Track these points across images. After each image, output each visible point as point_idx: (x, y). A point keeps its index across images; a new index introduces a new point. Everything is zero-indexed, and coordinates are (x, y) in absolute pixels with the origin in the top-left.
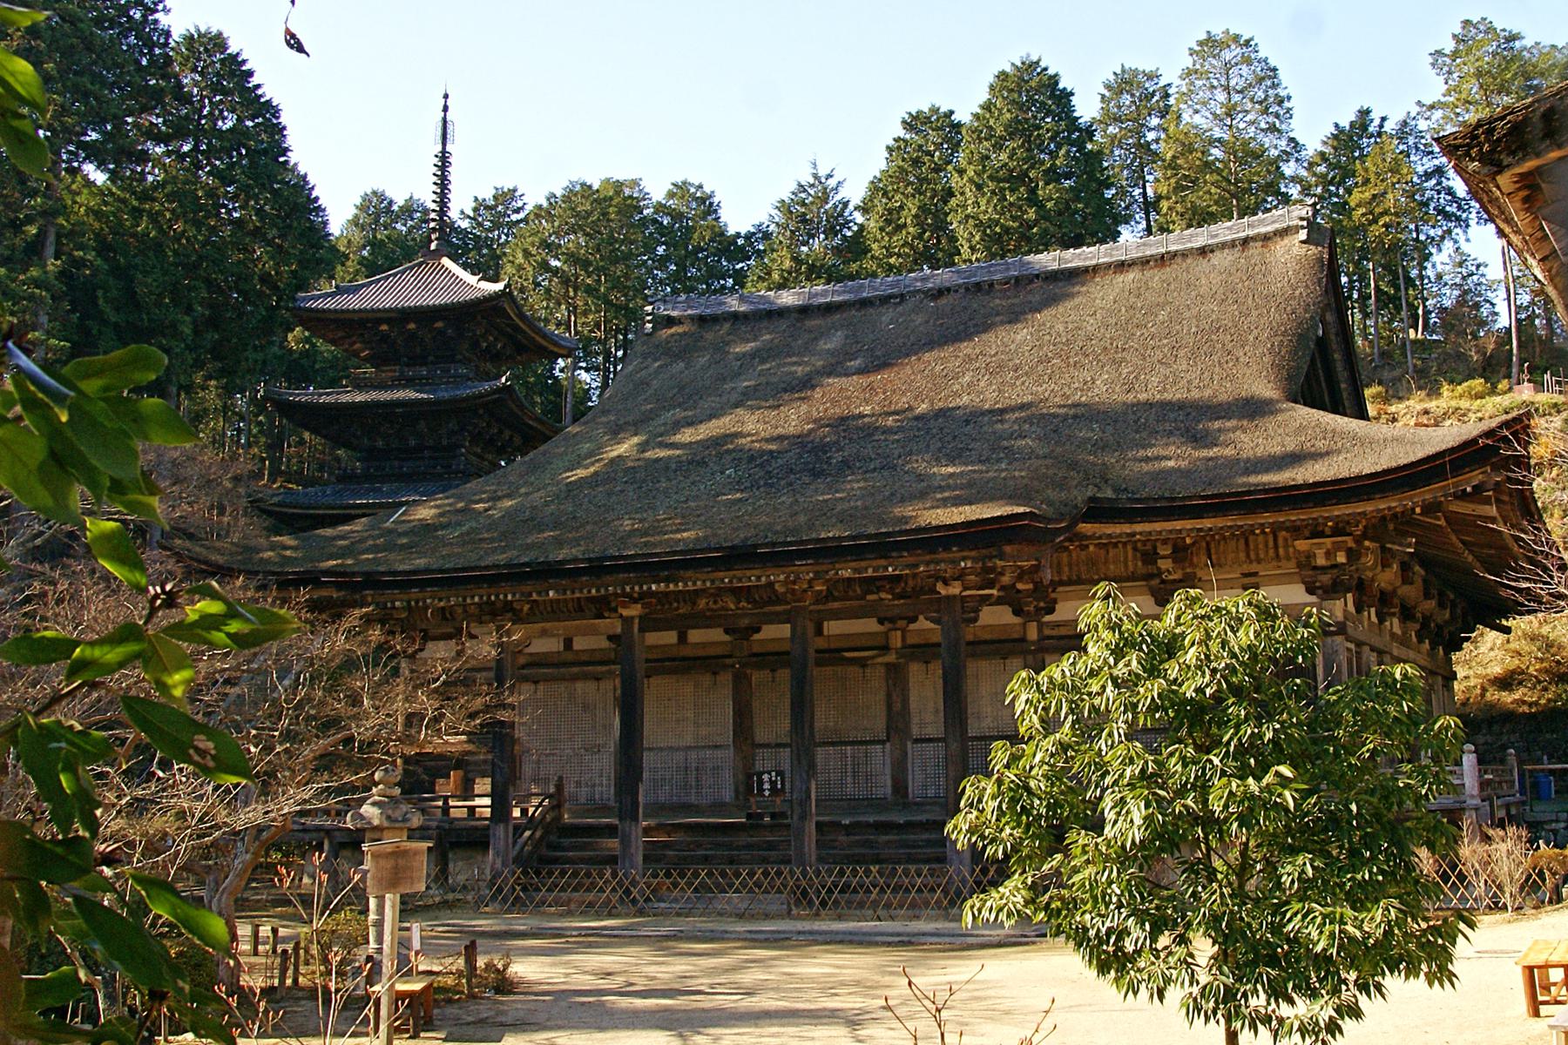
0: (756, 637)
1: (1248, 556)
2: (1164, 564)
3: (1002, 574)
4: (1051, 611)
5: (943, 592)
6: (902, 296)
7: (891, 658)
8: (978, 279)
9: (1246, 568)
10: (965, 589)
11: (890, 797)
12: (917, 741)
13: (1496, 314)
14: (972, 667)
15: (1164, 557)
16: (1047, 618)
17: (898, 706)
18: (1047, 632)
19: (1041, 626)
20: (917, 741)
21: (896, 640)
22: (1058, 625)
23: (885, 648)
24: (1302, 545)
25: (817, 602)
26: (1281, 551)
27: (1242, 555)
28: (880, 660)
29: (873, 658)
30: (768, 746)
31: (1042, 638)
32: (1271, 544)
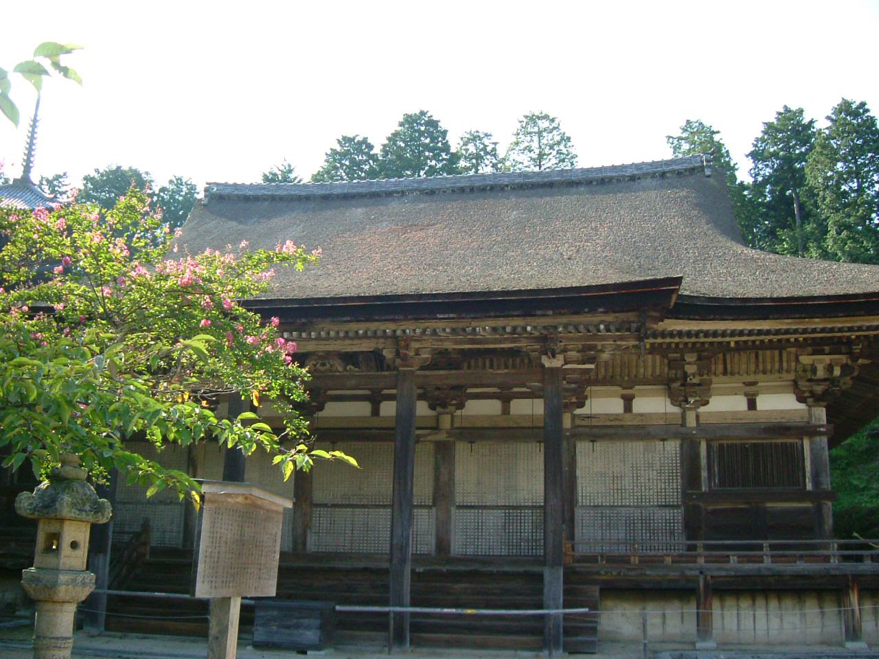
0: (321, 414)
1: (757, 366)
2: (691, 369)
3: (602, 351)
4: (581, 405)
5: (547, 365)
6: (403, 192)
7: (442, 437)
8: (462, 185)
9: (751, 378)
10: (566, 363)
11: (433, 553)
12: (459, 507)
13: (554, 356)
14: (314, 502)
15: (689, 363)
16: (578, 411)
17: (444, 478)
18: (578, 422)
19: (574, 417)
20: (459, 507)
21: (446, 422)
22: (589, 417)
23: (436, 428)
24: (806, 360)
25: (422, 368)
26: (785, 364)
27: (753, 367)
28: (432, 438)
29: (425, 436)
30: (326, 505)
31: (575, 427)
32: (777, 359)
